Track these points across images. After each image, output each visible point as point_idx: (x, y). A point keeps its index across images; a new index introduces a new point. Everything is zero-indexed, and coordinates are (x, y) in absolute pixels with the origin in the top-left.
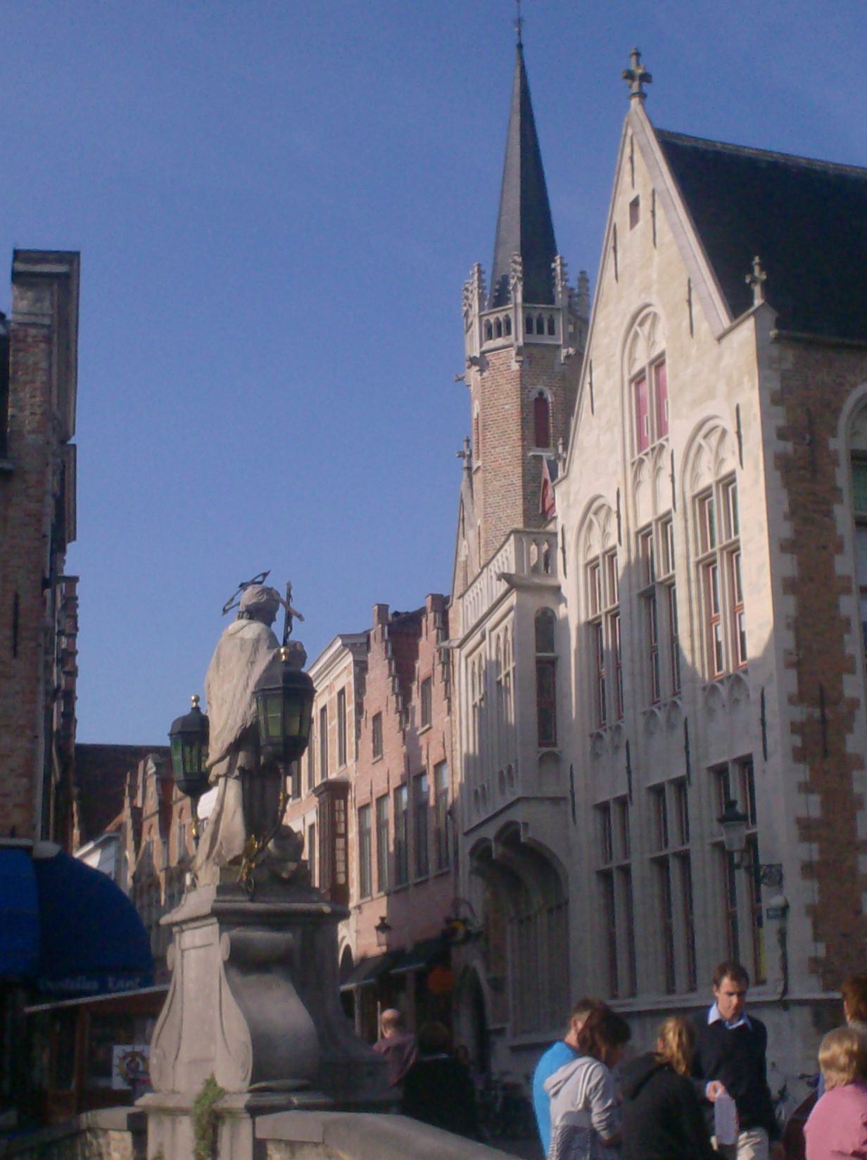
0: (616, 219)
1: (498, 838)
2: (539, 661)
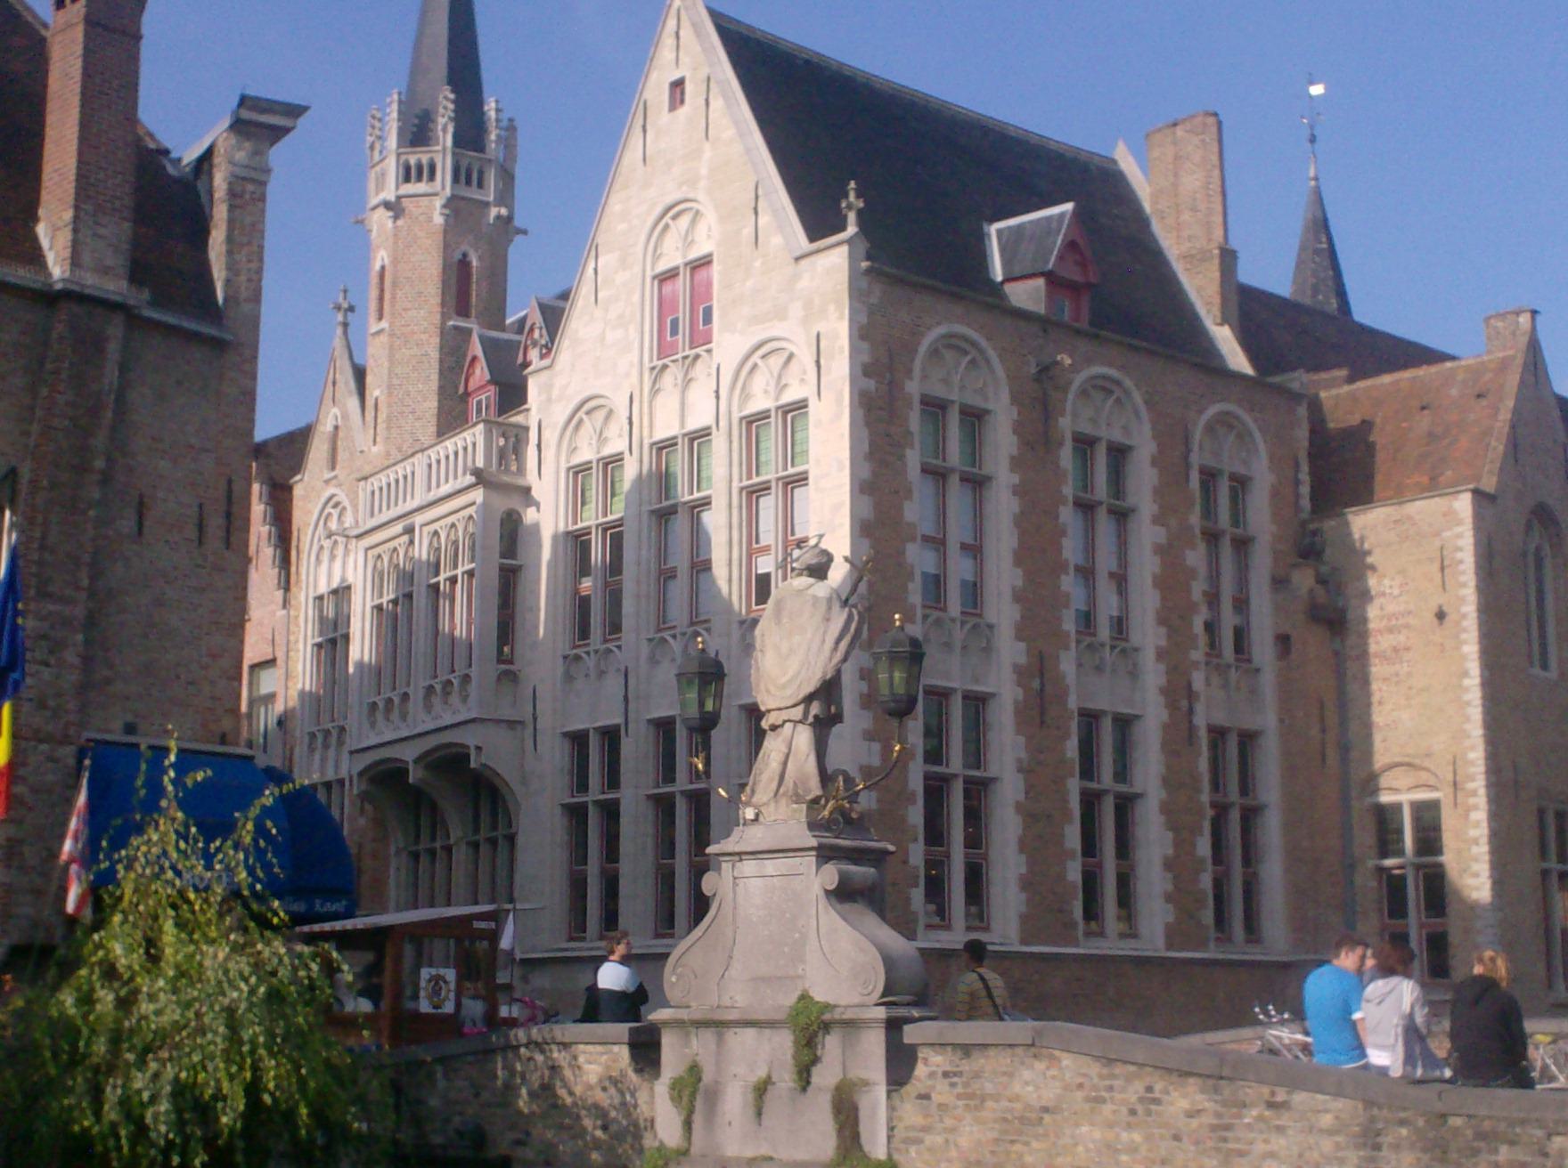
0: (648, 95)
1: (417, 761)
2: (502, 569)
